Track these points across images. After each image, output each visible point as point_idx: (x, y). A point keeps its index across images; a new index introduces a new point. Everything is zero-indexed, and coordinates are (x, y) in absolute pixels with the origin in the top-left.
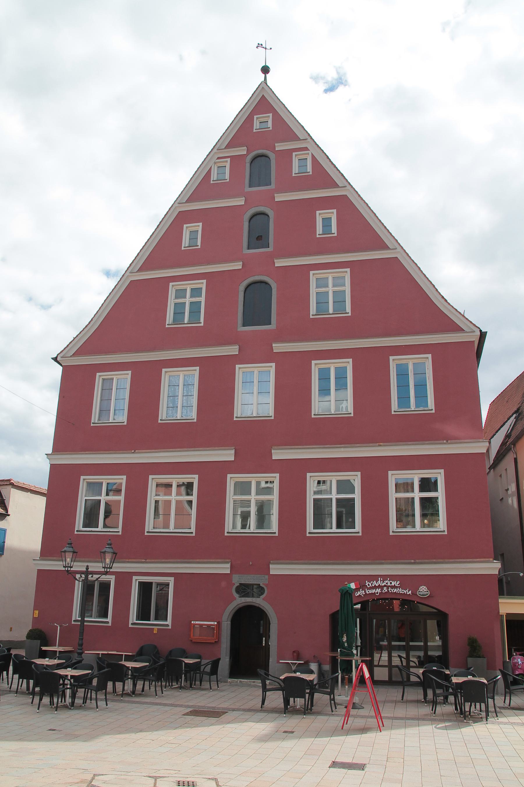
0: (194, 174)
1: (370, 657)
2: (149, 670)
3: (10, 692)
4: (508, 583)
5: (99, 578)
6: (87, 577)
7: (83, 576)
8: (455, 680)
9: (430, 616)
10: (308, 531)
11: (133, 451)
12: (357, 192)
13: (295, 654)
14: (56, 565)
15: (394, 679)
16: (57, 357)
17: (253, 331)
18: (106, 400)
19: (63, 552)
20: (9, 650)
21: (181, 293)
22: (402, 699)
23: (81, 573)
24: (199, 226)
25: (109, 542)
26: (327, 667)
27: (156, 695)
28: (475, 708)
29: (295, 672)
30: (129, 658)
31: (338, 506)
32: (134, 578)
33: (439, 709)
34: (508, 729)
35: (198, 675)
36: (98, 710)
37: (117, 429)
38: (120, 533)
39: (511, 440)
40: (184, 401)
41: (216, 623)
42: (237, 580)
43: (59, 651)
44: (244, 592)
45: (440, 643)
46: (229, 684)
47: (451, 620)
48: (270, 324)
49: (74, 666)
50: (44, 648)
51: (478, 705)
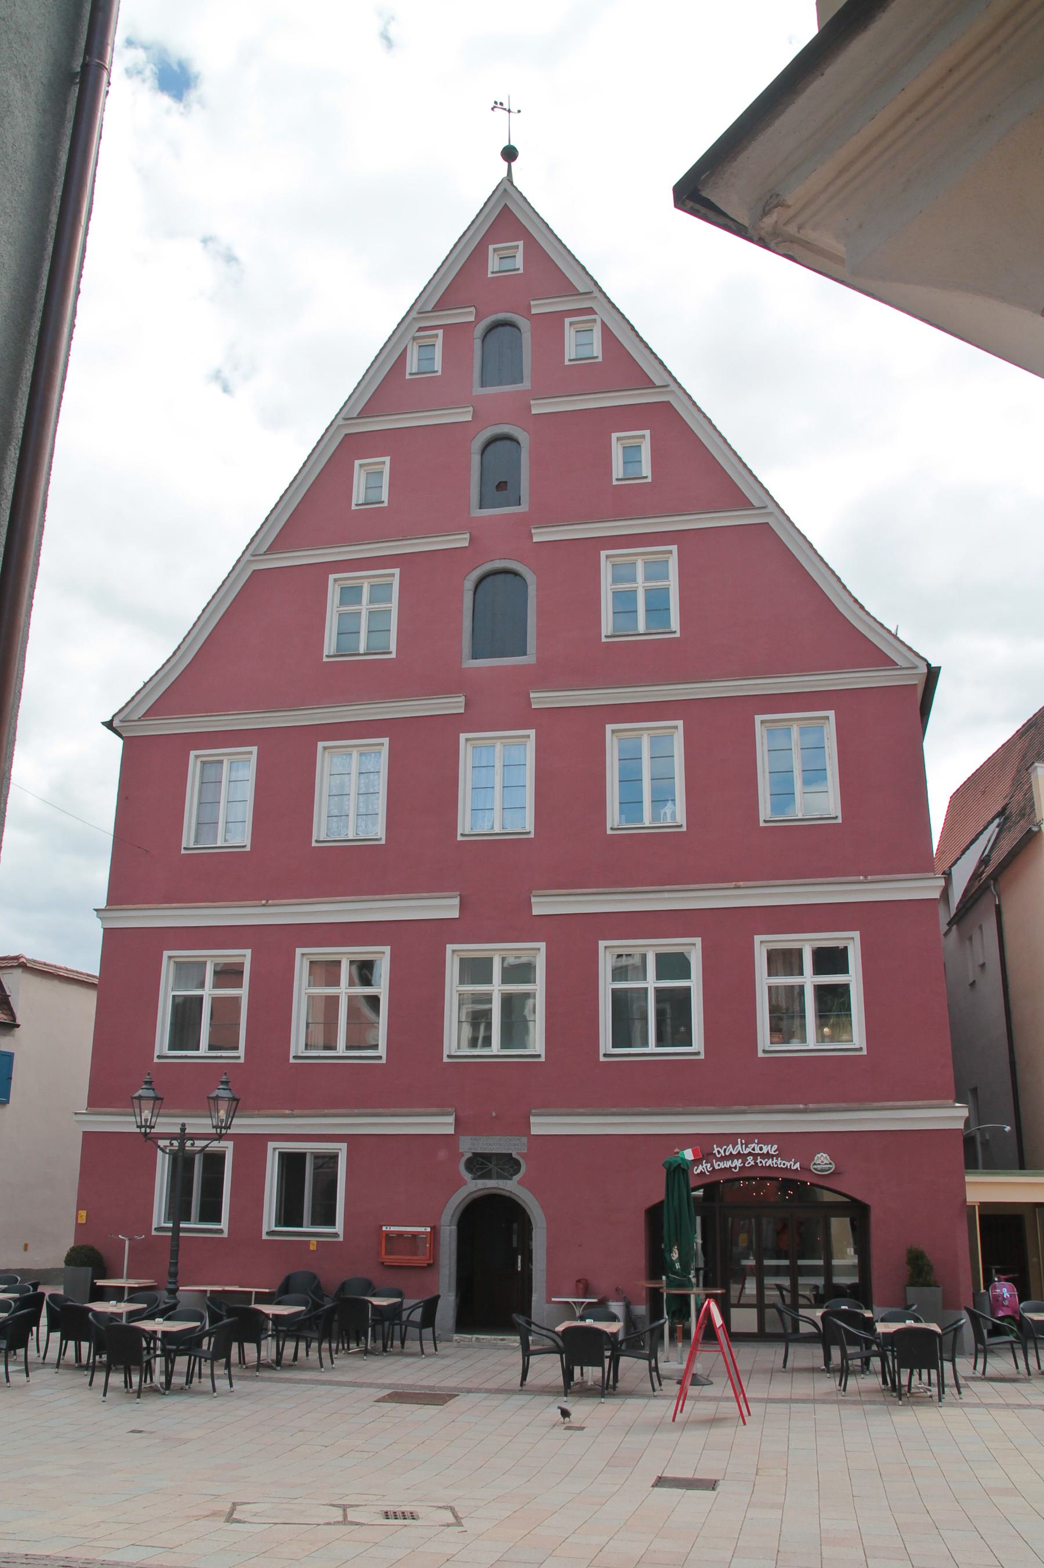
0: (374, 362)
1: (722, 1288)
2: (309, 1319)
3: (44, 1364)
4: (985, 1144)
5: (207, 1146)
6: (182, 1145)
7: (176, 1143)
8: (881, 1328)
9: (837, 1209)
10: (602, 1052)
11: (264, 902)
12: (690, 397)
13: (581, 1286)
14: (123, 1123)
15: (768, 1330)
16: (112, 721)
17: (492, 668)
18: (209, 803)
19: (136, 1098)
20: (35, 1286)
21: (350, 595)
22: (784, 1366)
23: (170, 1137)
24: (384, 463)
25: (224, 1078)
26: (641, 1310)
27: (322, 1366)
28: (919, 1380)
29: (582, 1318)
30: (262, 1298)
31: (658, 1001)
32: (271, 1145)
33: (852, 1382)
34: (978, 1415)
35: (397, 1328)
36: (215, 1394)
37: (231, 858)
38: (242, 1061)
39: (989, 870)
40: (361, 804)
41: (429, 1229)
42: (468, 1146)
43: (130, 1288)
44: (482, 1169)
45: (855, 1261)
46: (455, 1344)
47: (875, 1216)
48: (525, 654)
49: (168, 1313)
50: (100, 1283)
51: (925, 1372)
